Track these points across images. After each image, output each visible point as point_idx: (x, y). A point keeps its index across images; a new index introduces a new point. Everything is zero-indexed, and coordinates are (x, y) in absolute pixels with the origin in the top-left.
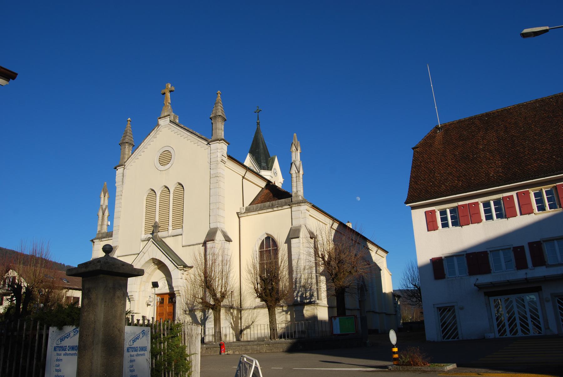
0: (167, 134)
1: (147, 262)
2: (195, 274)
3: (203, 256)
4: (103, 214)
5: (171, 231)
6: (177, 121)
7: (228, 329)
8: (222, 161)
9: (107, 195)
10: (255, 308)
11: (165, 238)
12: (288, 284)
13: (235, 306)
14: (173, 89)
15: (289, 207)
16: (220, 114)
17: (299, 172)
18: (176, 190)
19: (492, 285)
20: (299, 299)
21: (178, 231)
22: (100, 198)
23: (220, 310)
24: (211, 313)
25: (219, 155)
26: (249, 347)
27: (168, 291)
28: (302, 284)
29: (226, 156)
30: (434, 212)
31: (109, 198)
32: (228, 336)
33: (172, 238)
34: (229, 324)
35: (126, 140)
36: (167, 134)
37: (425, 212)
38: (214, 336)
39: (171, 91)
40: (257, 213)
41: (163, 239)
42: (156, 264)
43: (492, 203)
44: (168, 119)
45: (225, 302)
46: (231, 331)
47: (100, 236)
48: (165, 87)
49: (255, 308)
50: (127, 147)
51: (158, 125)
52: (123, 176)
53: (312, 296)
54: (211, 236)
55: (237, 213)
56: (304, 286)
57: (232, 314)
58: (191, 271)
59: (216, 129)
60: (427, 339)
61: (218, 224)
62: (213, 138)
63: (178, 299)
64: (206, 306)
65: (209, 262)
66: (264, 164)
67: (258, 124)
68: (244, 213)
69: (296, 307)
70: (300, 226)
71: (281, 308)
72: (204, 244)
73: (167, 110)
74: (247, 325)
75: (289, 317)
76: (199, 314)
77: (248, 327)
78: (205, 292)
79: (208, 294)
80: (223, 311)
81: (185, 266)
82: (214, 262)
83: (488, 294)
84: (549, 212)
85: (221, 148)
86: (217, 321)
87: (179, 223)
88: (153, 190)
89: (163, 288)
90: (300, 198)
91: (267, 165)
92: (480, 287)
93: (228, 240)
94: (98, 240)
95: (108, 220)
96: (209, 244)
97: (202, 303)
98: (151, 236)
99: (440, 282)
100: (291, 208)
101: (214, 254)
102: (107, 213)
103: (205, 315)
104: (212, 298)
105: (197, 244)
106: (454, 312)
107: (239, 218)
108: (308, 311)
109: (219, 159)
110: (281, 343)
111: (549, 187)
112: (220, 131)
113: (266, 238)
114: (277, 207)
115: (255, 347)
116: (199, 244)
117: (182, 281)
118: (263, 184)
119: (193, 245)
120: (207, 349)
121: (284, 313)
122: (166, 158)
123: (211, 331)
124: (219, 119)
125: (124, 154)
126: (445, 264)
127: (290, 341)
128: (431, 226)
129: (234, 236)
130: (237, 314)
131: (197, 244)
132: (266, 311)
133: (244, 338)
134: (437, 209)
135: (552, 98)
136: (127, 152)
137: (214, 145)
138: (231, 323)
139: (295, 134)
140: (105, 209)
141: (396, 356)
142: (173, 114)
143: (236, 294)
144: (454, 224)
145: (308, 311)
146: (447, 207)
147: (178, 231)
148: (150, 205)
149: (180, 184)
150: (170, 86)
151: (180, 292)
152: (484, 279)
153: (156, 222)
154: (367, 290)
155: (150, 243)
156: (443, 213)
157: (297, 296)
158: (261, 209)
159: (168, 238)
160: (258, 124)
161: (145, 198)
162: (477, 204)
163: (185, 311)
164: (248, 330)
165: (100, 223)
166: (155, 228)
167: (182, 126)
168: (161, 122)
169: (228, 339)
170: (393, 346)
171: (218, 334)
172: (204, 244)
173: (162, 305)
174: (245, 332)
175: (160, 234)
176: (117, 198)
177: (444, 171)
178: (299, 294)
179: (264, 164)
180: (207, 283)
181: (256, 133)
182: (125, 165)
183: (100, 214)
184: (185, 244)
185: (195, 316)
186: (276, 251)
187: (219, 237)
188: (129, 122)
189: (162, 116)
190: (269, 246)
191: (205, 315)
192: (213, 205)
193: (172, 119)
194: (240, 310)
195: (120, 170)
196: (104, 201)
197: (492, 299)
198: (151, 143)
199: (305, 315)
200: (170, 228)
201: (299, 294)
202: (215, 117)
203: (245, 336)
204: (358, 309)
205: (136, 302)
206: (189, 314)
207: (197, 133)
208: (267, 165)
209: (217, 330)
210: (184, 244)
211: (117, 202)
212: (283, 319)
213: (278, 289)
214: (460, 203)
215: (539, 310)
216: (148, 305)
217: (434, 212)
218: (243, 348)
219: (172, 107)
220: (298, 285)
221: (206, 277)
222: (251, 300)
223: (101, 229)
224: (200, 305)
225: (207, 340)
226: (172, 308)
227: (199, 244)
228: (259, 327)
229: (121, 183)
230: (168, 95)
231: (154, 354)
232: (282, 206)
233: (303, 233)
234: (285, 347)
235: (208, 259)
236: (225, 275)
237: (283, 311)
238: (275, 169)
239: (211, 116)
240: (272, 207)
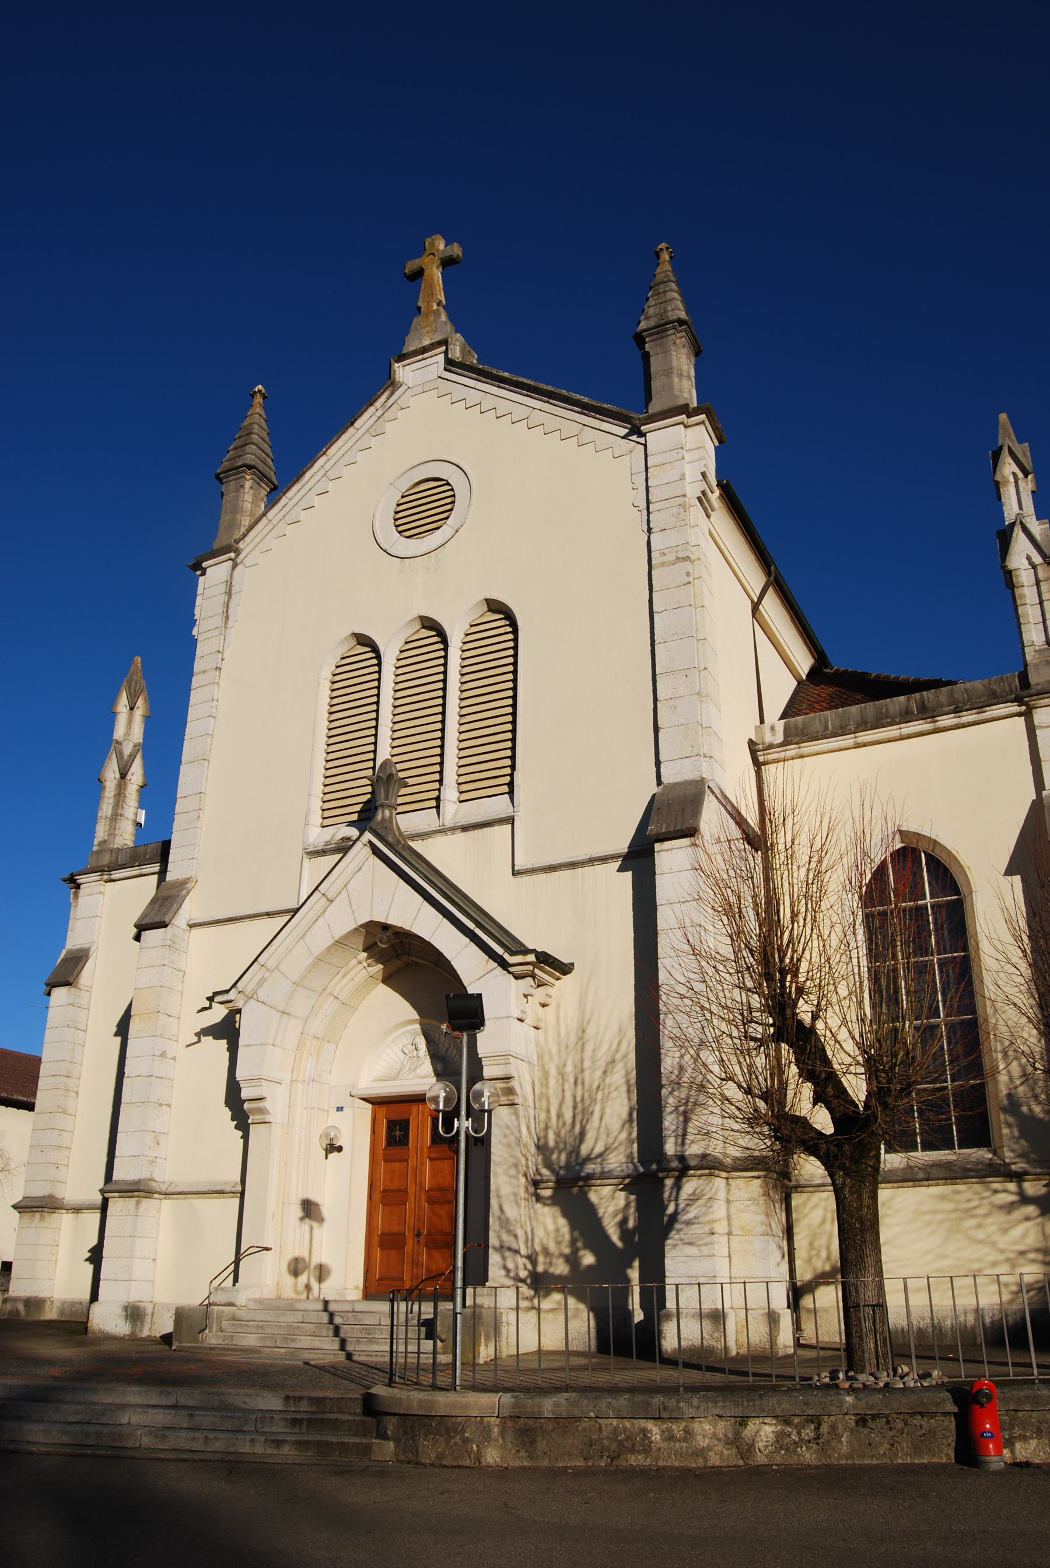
1: (340, 943)
4: (123, 775)
5: (453, 810)
9: (140, 703)
14: (456, 250)
15: (1015, 708)
18: (474, 634)
21: (499, 806)
22: (114, 715)
31: (147, 719)
33: (460, 836)
35: (249, 459)
36: (432, 413)
40: (848, 740)
41: (415, 845)
47: (106, 859)
50: (248, 484)
52: (229, 593)
55: (751, 743)
61: (704, 764)
68: (781, 745)
71: (1012, 1186)
72: (639, 859)
73: (434, 323)
85: (688, 450)
94: (95, 877)
95: (141, 805)
100: (1028, 715)
102: (136, 775)
105: (592, 861)
107: (758, 764)
114: (957, 711)
116: (604, 859)
119: (572, 865)
120: (862, 1421)
121: (1031, 1210)
122: (426, 507)
125: (236, 509)
131: (592, 861)
136: (247, 506)
137: (662, 437)
139: (1003, 417)
140: (132, 757)
147: (499, 806)
151: (514, 1084)
159: (439, 839)
163: (536, 1184)
165: (106, 809)
168: (403, 372)
172: (639, 859)
173: (395, 1151)
175: (407, 823)
176: (196, 681)
182: (238, 552)
183: (111, 774)
185: (591, 1209)
188: (259, 399)
189: (410, 347)
195: (216, 572)
196: (129, 725)
198: (346, 471)
200: (450, 793)
205: (276, 1130)
211: (195, 697)
223: (112, 833)
227: (604, 859)
229: (218, 621)
230: (436, 274)
232: (980, 707)
237: (1025, 1199)
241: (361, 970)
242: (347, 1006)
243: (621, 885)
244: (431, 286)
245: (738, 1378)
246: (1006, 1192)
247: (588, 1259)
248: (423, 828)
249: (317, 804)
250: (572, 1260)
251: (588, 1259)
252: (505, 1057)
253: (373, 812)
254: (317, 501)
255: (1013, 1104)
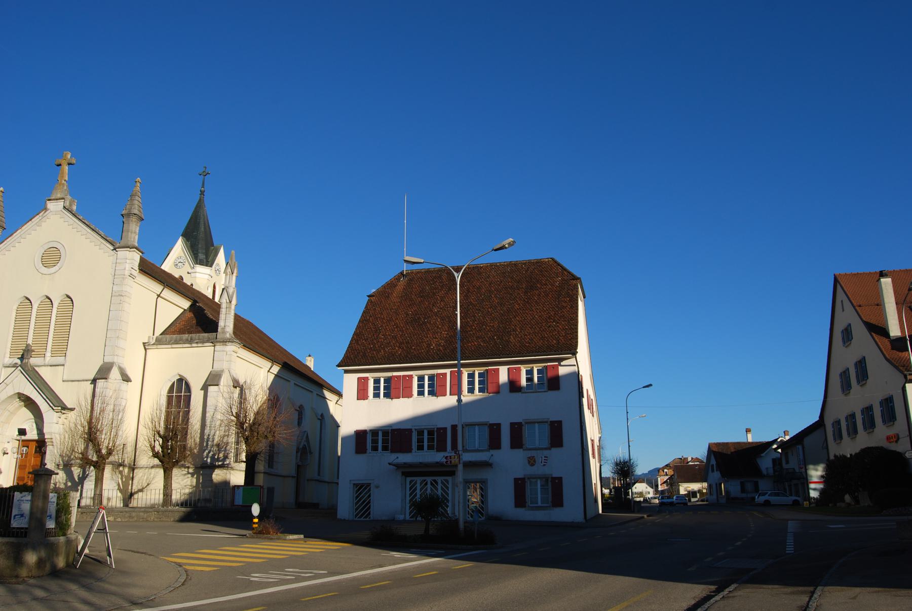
0: (56, 224)
2: (75, 420)
3: (89, 402)
5: (48, 359)
6: (74, 208)
7: (115, 492)
8: (131, 276)
10: (152, 467)
11: (39, 366)
12: (198, 440)
13: (126, 462)
14: (74, 161)
16: (136, 211)
17: (230, 302)
19: (410, 465)
20: (209, 460)
21: (60, 360)
23: (104, 469)
24: (92, 471)
25: (128, 267)
26: (134, 514)
27: (36, 437)
28: (215, 442)
29: (137, 268)
30: (367, 379)
32: (114, 500)
34: (116, 485)
36: (56, 224)
37: (358, 379)
38: (94, 499)
39: (69, 164)
40: (169, 346)
41: (36, 368)
42: (23, 401)
43: (426, 378)
44: (61, 204)
45: (111, 459)
46: (119, 494)
48: (62, 157)
49: (152, 467)
51: (46, 209)
53: (226, 457)
54: (103, 372)
55: (144, 344)
56: (218, 445)
57: (121, 472)
58: (71, 415)
59: (128, 231)
60: (339, 516)
62: (123, 243)
63: (49, 449)
64: (86, 462)
65: (97, 410)
66: (201, 256)
67: (202, 193)
69: (204, 469)
70: (223, 371)
72: (94, 381)
74: (140, 487)
75: (195, 480)
76: (76, 471)
77: (141, 490)
78: (87, 446)
79: (91, 447)
80: (108, 470)
81: (64, 408)
82: (102, 411)
83: (406, 474)
84: (477, 395)
86: (99, 481)
87: (62, 349)
88: (27, 299)
89: (32, 434)
90: (228, 336)
91: (207, 258)
92: (398, 466)
93: (126, 379)
96: (100, 383)
97: (81, 459)
98: (19, 362)
99: (361, 457)
101: (103, 403)
103: (84, 472)
104: (94, 453)
106: (370, 490)
107: (146, 349)
108: (218, 475)
109: (127, 273)
110: (172, 511)
111: (483, 369)
112: (133, 235)
113: (178, 380)
115: (142, 514)
117: (58, 428)
118: (186, 304)
122: (51, 257)
123: (89, 493)
124: (134, 219)
126: (369, 438)
127: (183, 509)
128: (362, 394)
129: (135, 374)
130: (129, 473)
132: (161, 471)
133: (134, 503)
134: (371, 376)
135: (525, 264)
137: (122, 253)
138: (119, 485)
139: (233, 252)
141: (255, 526)
142: (69, 197)
143: (130, 449)
144: (386, 395)
145: (218, 475)
146: (382, 376)
147: (60, 360)
148: (22, 319)
149: (68, 297)
150: (69, 157)
152: (404, 458)
153: (28, 345)
154: (311, 453)
155: (17, 372)
156: (377, 381)
157: (207, 457)
158: (176, 342)
160: (202, 193)
161: (15, 308)
162: (411, 377)
164: (140, 494)
166: (26, 354)
167: (81, 217)
168: (51, 205)
169: (114, 504)
170: (254, 517)
171: (98, 497)
172: (94, 381)
174: (136, 496)
175: (33, 361)
177: (392, 334)
178: (210, 455)
179: (201, 256)
180: (91, 435)
181: (197, 207)
184: (68, 379)
185: (72, 472)
186: (188, 399)
187: (115, 374)
190: (179, 393)
191: (84, 472)
192: (112, 331)
193: (67, 204)
194: (133, 468)
197: (409, 479)
199: (215, 480)
200: (48, 354)
201: (210, 455)
202: (129, 215)
203: (135, 502)
204: (293, 477)
206: (63, 469)
207: (101, 233)
208: (207, 258)
209: (98, 492)
210: (65, 378)
212: (183, 483)
213: (185, 447)
214: (395, 374)
215: (450, 495)
216: (5, 453)
217: (367, 379)
218: (127, 515)
219: (69, 187)
220: (210, 443)
221: (90, 428)
222: (146, 459)
224: (78, 461)
225: (83, 503)
226: (39, 459)
228: (153, 491)
230: (66, 168)
231: (57, 504)
232: (203, 343)
233: (225, 381)
234: (177, 516)
235: (95, 408)
236: (116, 425)
237: (188, 473)
238: (218, 265)
239: (124, 212)
240: (190, 342)
241: (17, 403)
242: (13, 413)
243: (89, 387)
244: (63, 173)
245: (643, 506)
246: (185, 471)
247: (69, 484)
248: (39, 364)
249: (8, 350)
250: (66, 484)
251: (69, 484)
252: (51, 433)
253: (24, 359)
254: (17, 245)
255: (191, 450)
